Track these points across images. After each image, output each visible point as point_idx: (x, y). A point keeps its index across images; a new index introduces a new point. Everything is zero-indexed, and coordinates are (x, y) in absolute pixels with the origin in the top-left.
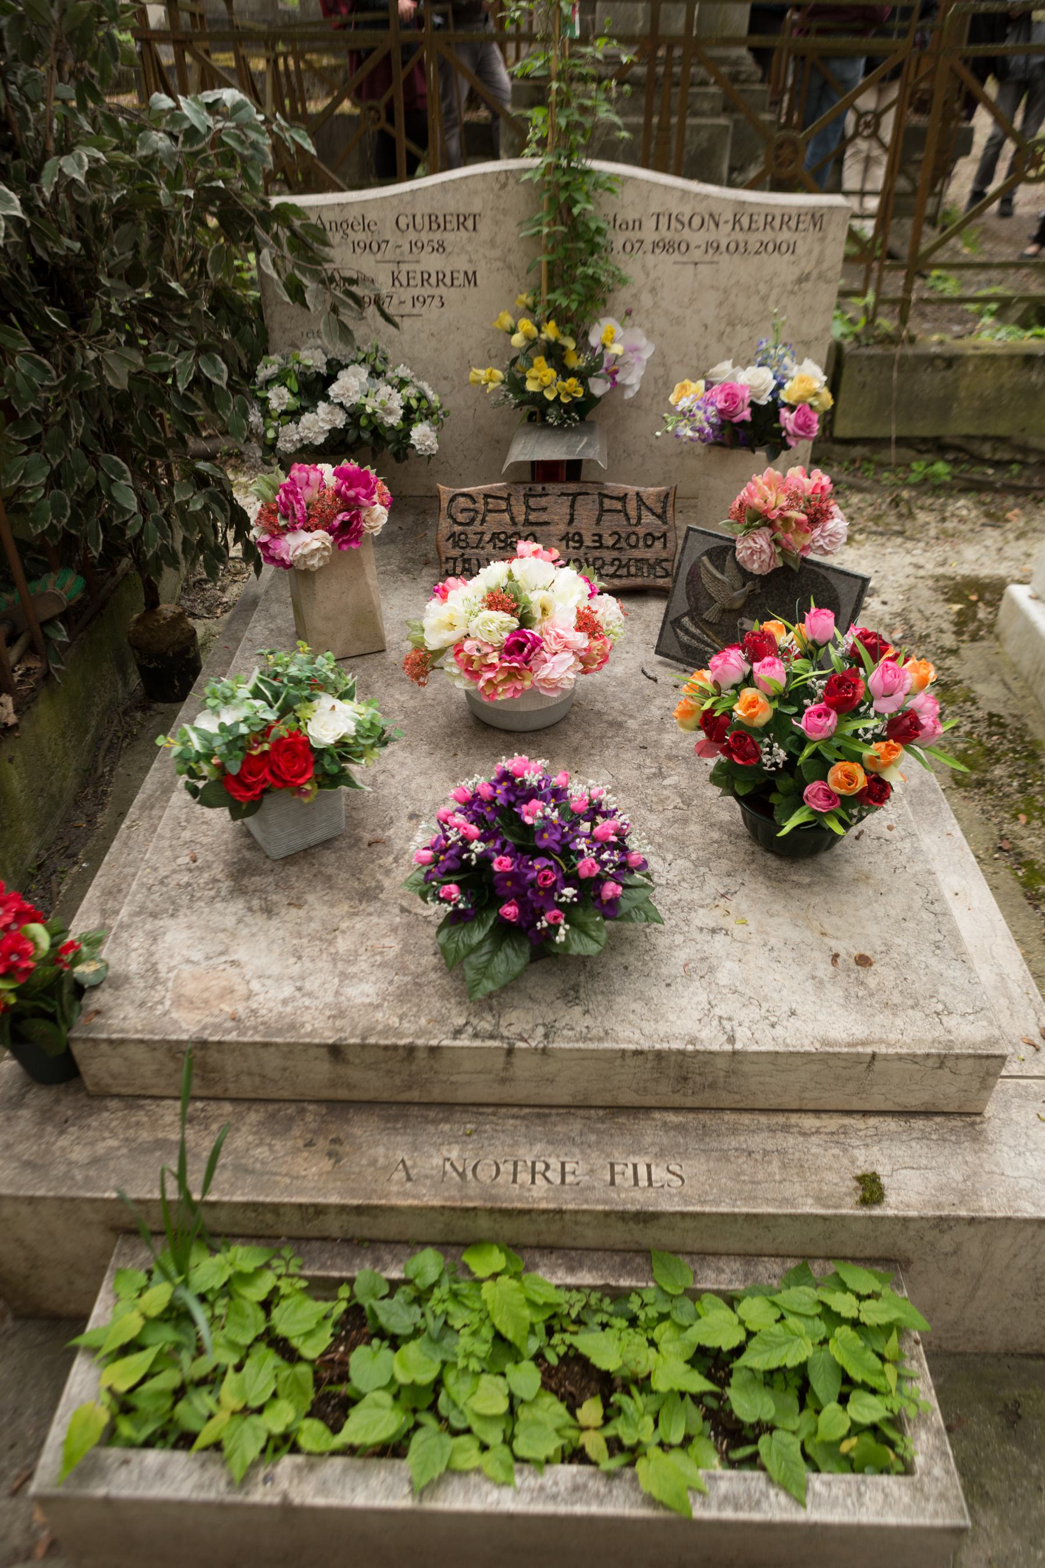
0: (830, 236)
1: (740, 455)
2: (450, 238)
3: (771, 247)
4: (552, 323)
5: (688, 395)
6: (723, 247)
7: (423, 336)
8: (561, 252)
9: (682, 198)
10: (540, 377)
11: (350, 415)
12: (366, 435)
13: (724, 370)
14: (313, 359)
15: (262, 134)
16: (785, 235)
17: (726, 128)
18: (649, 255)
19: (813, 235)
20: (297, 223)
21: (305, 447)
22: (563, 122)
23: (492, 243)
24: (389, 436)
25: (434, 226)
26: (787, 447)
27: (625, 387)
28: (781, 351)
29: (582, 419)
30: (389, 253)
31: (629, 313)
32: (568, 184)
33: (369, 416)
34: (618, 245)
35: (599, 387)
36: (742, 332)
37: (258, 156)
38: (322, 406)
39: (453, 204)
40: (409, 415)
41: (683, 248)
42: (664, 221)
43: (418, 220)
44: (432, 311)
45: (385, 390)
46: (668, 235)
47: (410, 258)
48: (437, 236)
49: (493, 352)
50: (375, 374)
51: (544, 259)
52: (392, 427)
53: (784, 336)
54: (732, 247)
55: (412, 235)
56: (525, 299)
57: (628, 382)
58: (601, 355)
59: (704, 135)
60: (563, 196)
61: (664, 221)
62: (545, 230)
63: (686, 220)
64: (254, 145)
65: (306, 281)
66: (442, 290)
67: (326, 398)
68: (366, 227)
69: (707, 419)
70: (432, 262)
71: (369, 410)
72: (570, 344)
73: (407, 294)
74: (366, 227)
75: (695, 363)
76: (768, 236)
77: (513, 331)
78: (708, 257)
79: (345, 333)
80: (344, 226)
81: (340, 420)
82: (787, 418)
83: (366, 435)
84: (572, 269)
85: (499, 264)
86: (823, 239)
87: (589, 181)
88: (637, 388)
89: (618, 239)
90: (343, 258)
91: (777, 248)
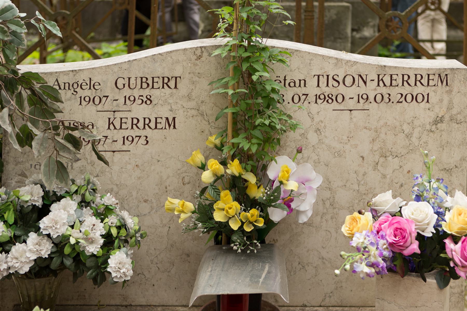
0: (455, 90)
1: (412, 281)
2: (156, 94)
3: (409, 98)
4: (236, 161)
5: (360, 229)
6: (371, 98)
7: (129, 167)
8: (243, 105)
9: (336, 65)
10: (226, 209)
11: (56, 245)
12: (68, 262)
13: (386, 200)
14: (31, 195)
15: (21, 26)
16: (419, 89)
17: (347, 8)
18: (313, 104)
19: (441, 89)
20: (37, 86)
21: (10, 275)
22: (244, 15)
23: (189, 97)
24: (89, 263)
25: (145, 85)
26: (456, 277)
27: (299, 212)
28: (435, 185)
29: (263, 242)
30: (108, 105)
31: (299, 151)
32: (249, 57)
33: (73, 247)
34: (288, 98)
35: (276, 215)
36: (394, 163)
37: (16, 40)
38: (33, 236)
39: (160, 70)
40: (109, 242)
41: (340, 99)
42: (323, 81)
43: (132, 81)
44: (138, 148)
45: (90, 220)
46: (327, 91)
47: (125, 108)
48: (146, 92)
49: (186, 180)
50: (84, 203)
51: (229, 111)
52: (93, 255)
53: (434, 170)
54: (379, 98)
55: (127, 92)
56: (214, 140)
57: (302, 208)
58: (278, 188)
59: (333, 12)
60: (245, 66)
61: (323, 81)
62: (231, 92)
63: (340, 79)
64: (14, 33)
65: (35, 131)
66: (148, 132)
67: (37, 230)
68: (92, 86)
69: (381, 255)
70: (141, 111)
71: (72, 241)
72: (252, 179)
73: (119, 135)
74: (92, 86)
75: (356, 187)
76: (406, 90)
77: (203, 167)
78: (360, 106)
79: (61, 170)
80: (74, 86)
81: (46, 250)
82: (453, 249)
83: (68, 262)
84: (252, 119)
85: (194, 112)
86: (450, 92)
87: (265, 55)
88: (310, 214)
89: (289, 93)
90: (71, 110)
91: (414, 98)
